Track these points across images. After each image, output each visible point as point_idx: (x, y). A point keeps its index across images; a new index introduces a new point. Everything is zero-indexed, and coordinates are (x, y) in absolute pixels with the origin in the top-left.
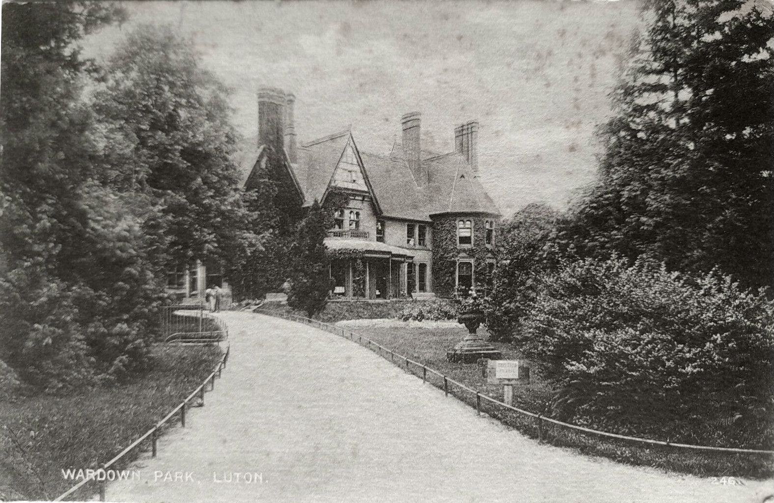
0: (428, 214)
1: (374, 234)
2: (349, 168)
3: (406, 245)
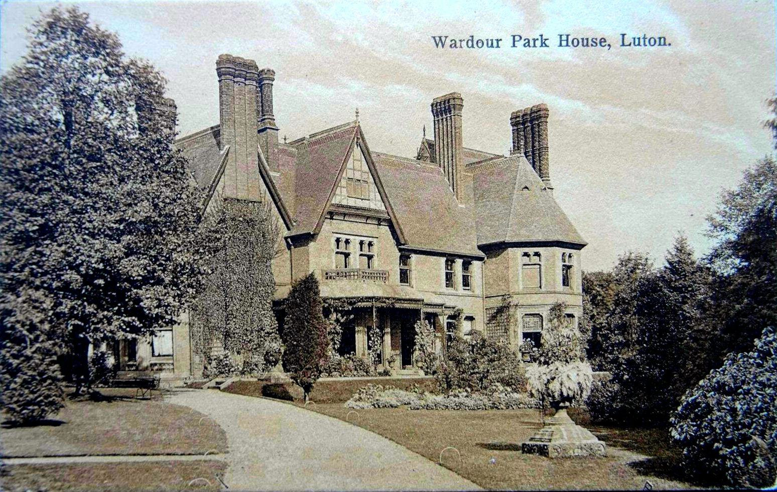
0: (475, 244)
1: (395, 268)
2: (358, 176)
3: (444, 289)
